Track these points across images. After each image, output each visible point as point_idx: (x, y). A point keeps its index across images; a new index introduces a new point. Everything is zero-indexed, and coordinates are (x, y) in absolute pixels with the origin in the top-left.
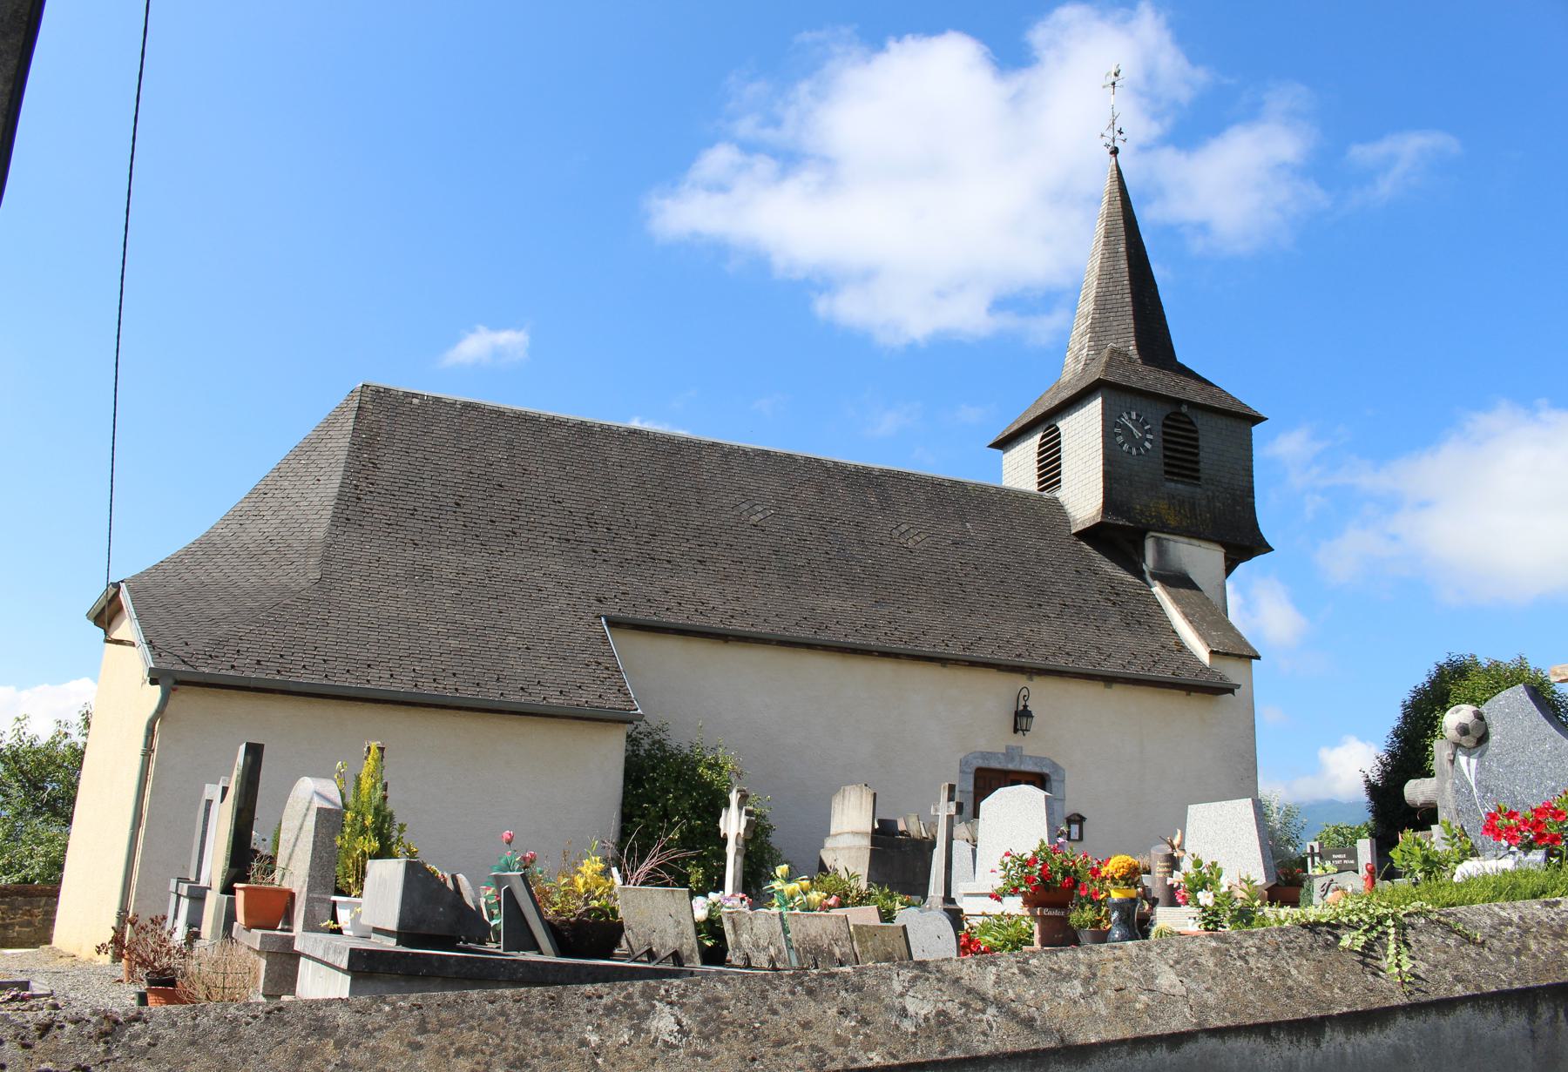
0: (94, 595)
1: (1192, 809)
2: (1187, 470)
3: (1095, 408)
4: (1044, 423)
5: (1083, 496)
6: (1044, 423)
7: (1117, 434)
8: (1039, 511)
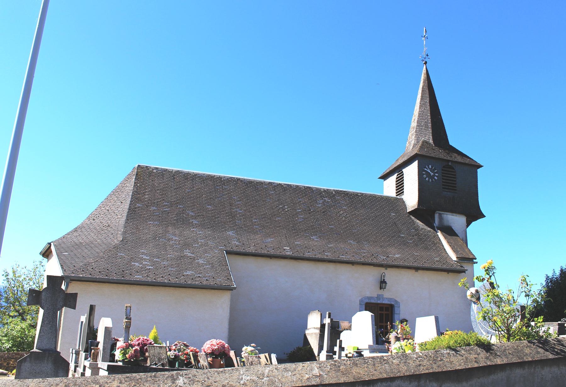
0: (42, 246)
1: (418, 320)
2: (452, 186)
3: (415, 164)
4: (398, 170)
5: (411, 199)
6: (398, 170)
7: (424, 174)
8: (396, 203)
